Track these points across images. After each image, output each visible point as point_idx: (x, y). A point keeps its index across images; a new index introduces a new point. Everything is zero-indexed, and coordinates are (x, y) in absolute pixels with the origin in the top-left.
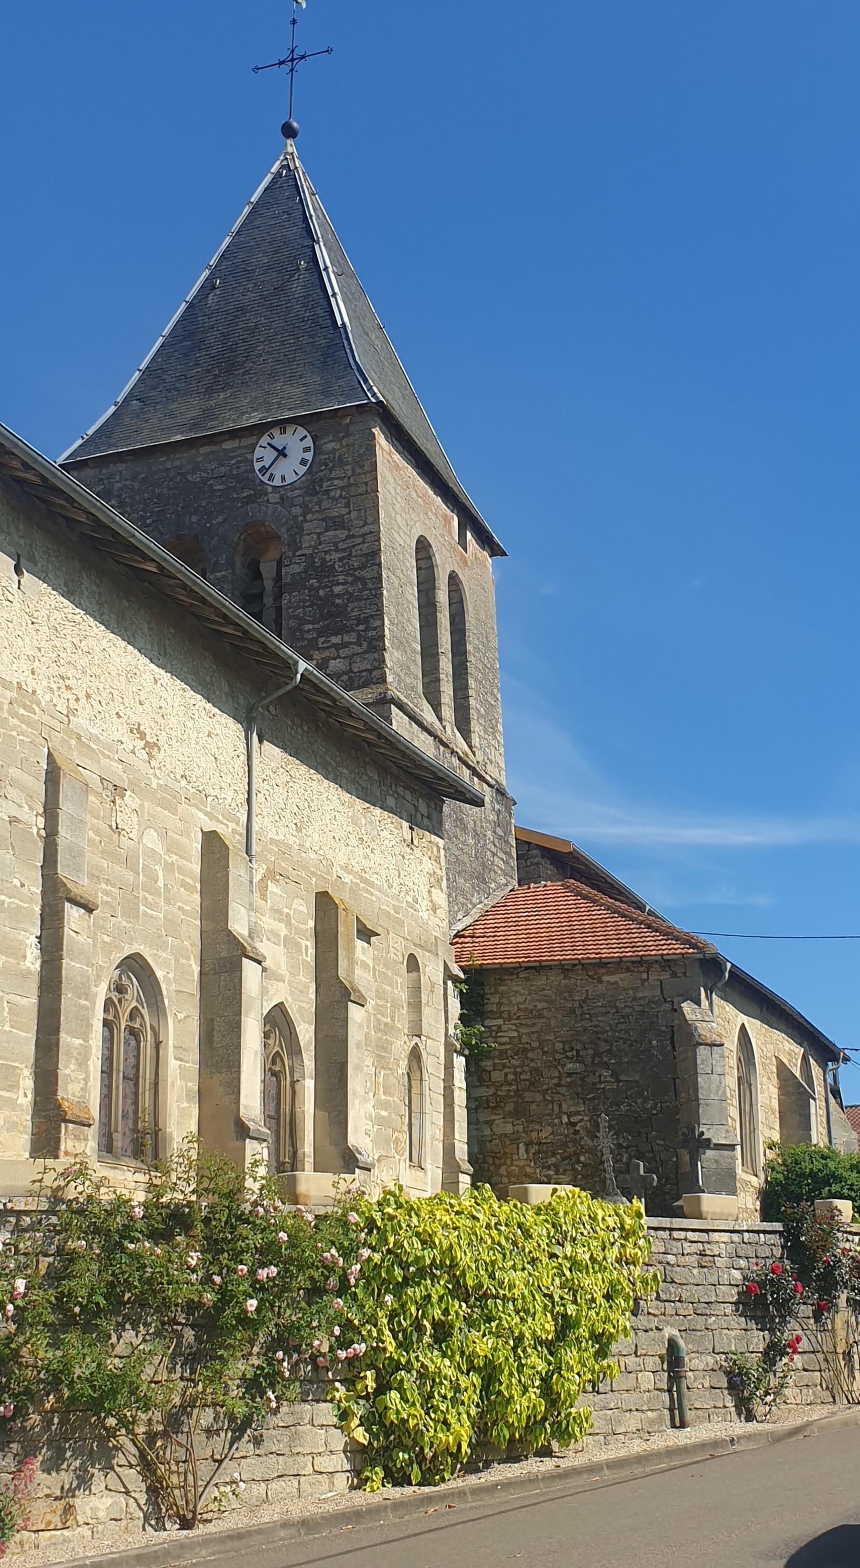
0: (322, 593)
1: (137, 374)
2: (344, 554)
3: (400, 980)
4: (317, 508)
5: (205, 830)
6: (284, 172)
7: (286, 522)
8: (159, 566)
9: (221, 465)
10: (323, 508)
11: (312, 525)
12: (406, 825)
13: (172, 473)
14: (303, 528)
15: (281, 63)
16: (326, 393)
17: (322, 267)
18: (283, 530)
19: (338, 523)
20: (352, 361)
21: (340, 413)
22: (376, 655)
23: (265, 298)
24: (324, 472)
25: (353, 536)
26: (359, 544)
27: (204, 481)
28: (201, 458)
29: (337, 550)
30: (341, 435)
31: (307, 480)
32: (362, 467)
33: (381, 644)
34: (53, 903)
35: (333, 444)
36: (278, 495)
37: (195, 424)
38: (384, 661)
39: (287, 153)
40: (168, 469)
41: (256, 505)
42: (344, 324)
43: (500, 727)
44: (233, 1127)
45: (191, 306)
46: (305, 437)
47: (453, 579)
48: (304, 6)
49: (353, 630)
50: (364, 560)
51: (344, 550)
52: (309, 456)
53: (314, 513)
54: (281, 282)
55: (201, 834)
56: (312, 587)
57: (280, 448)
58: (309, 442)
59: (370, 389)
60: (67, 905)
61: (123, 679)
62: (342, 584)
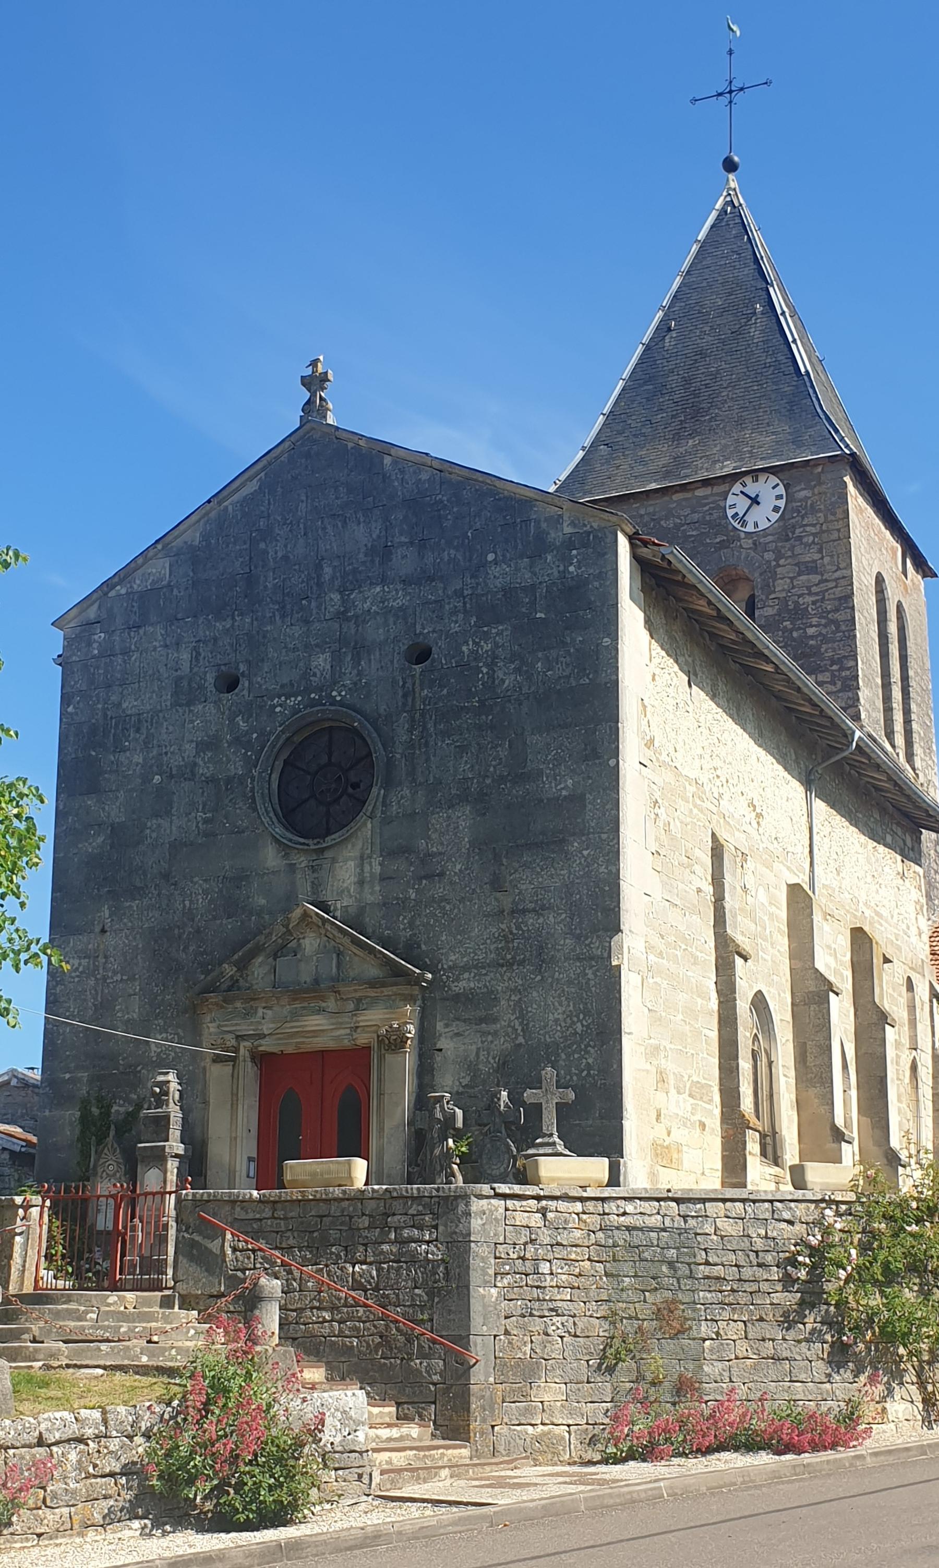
0: (795, 634)
1: (601, 419)
2: (817, 598)
3: (902, 1001)
4: (789, 553)
5: (789, 883)
6: (729, 209)
7: (759, 567)
8: (777, 667)
9: (693, 512)
10: (796, 553)
11: (785, 569)
12: (899, 858)
13: (646, 519)
14: (776, 572)
15: (720, 94)
16: (798, 443)
17: (779, 312)
18: (757, 575)
19: (812, 568)
20: (819, 410)
21: (812, 463)
22: (850, 694)
23: (723, 342)
24: (797, 519)
25: (827, 581)
26: (832, 588)
27: (677, 527)
28: (674, 505)
29: (810, 594)
30: (813, 483)
31: (779, 527)
32: (834, 514)
33: (855, 684)
34: (725, 955)
35: (805, 492)
36: (750, 541)
37: (668, 472)
38: (858, 700)
39: (729, 189)
40: (642, 516)
41: (729, 550)
42: (807, 371)
43: (934, 748)
44: (829, 1132)
45: (648, 348)
46: (778, 485)
47: (899, 606)
48: (738, 33)
49: (827, 670)
50: (837, 603)
51: (817, 594)
52: (782, 503)
53: (787, 558)
54: (738, 326)
55: (785, 886)
56: (785, 630)
57: (753, 496)
58: (781, 490)
59: (842, 439)
60: (736, 957)
61: (743, 762)
62: (815, 626)
